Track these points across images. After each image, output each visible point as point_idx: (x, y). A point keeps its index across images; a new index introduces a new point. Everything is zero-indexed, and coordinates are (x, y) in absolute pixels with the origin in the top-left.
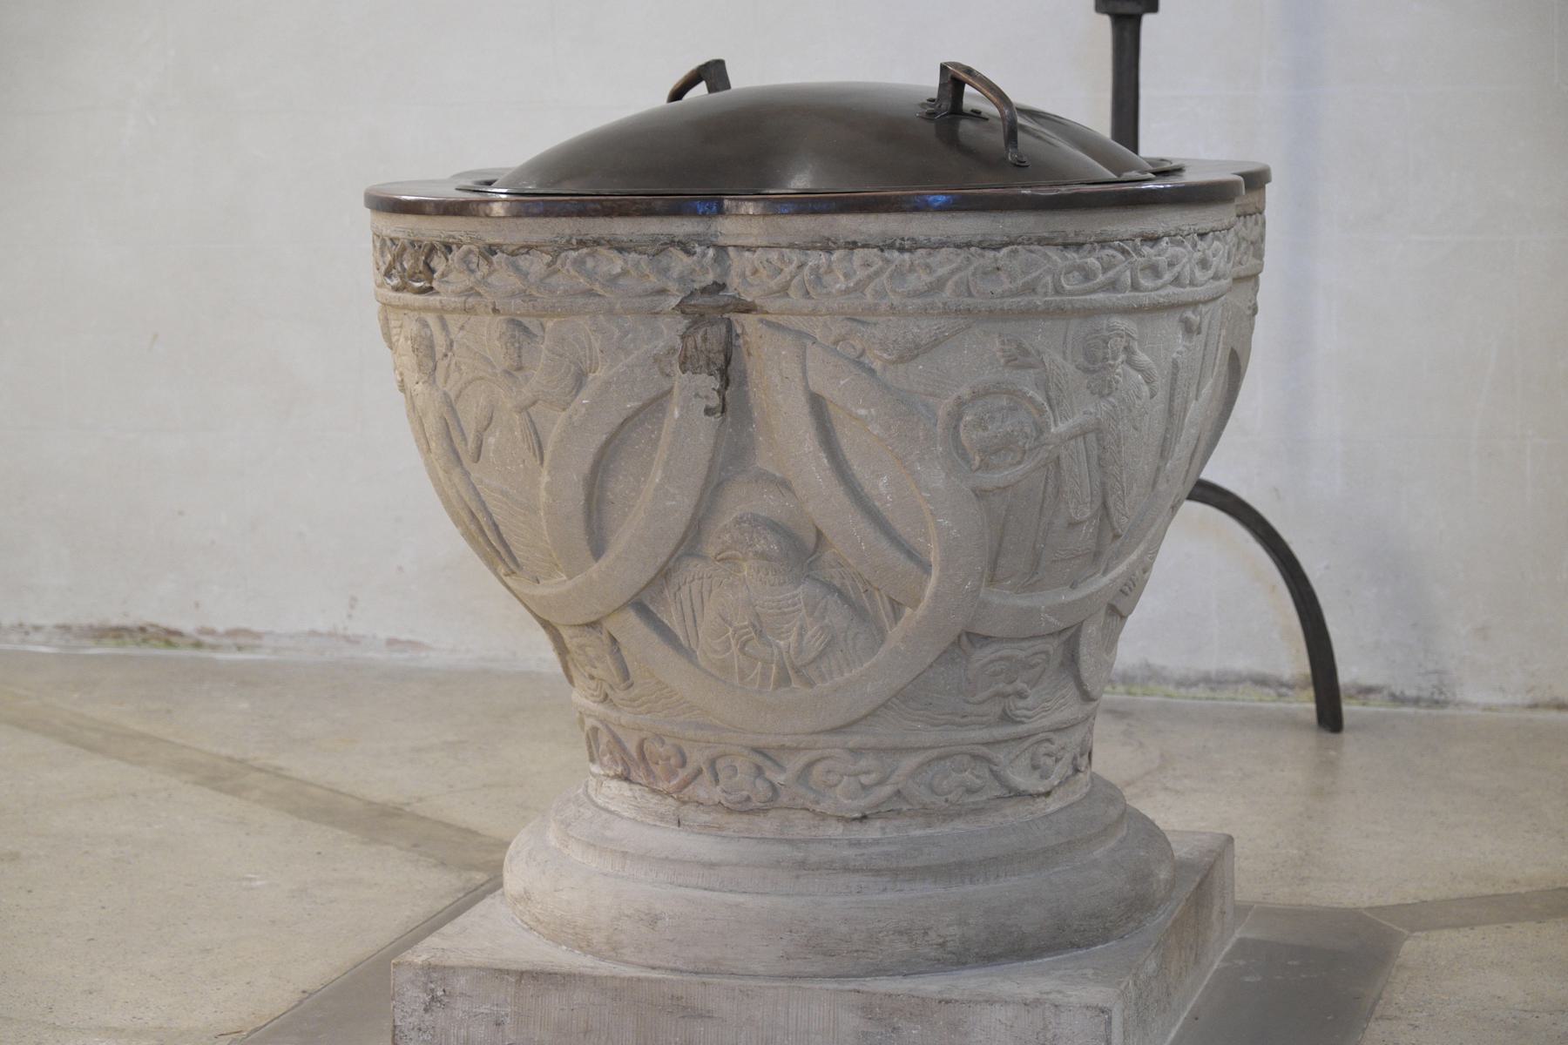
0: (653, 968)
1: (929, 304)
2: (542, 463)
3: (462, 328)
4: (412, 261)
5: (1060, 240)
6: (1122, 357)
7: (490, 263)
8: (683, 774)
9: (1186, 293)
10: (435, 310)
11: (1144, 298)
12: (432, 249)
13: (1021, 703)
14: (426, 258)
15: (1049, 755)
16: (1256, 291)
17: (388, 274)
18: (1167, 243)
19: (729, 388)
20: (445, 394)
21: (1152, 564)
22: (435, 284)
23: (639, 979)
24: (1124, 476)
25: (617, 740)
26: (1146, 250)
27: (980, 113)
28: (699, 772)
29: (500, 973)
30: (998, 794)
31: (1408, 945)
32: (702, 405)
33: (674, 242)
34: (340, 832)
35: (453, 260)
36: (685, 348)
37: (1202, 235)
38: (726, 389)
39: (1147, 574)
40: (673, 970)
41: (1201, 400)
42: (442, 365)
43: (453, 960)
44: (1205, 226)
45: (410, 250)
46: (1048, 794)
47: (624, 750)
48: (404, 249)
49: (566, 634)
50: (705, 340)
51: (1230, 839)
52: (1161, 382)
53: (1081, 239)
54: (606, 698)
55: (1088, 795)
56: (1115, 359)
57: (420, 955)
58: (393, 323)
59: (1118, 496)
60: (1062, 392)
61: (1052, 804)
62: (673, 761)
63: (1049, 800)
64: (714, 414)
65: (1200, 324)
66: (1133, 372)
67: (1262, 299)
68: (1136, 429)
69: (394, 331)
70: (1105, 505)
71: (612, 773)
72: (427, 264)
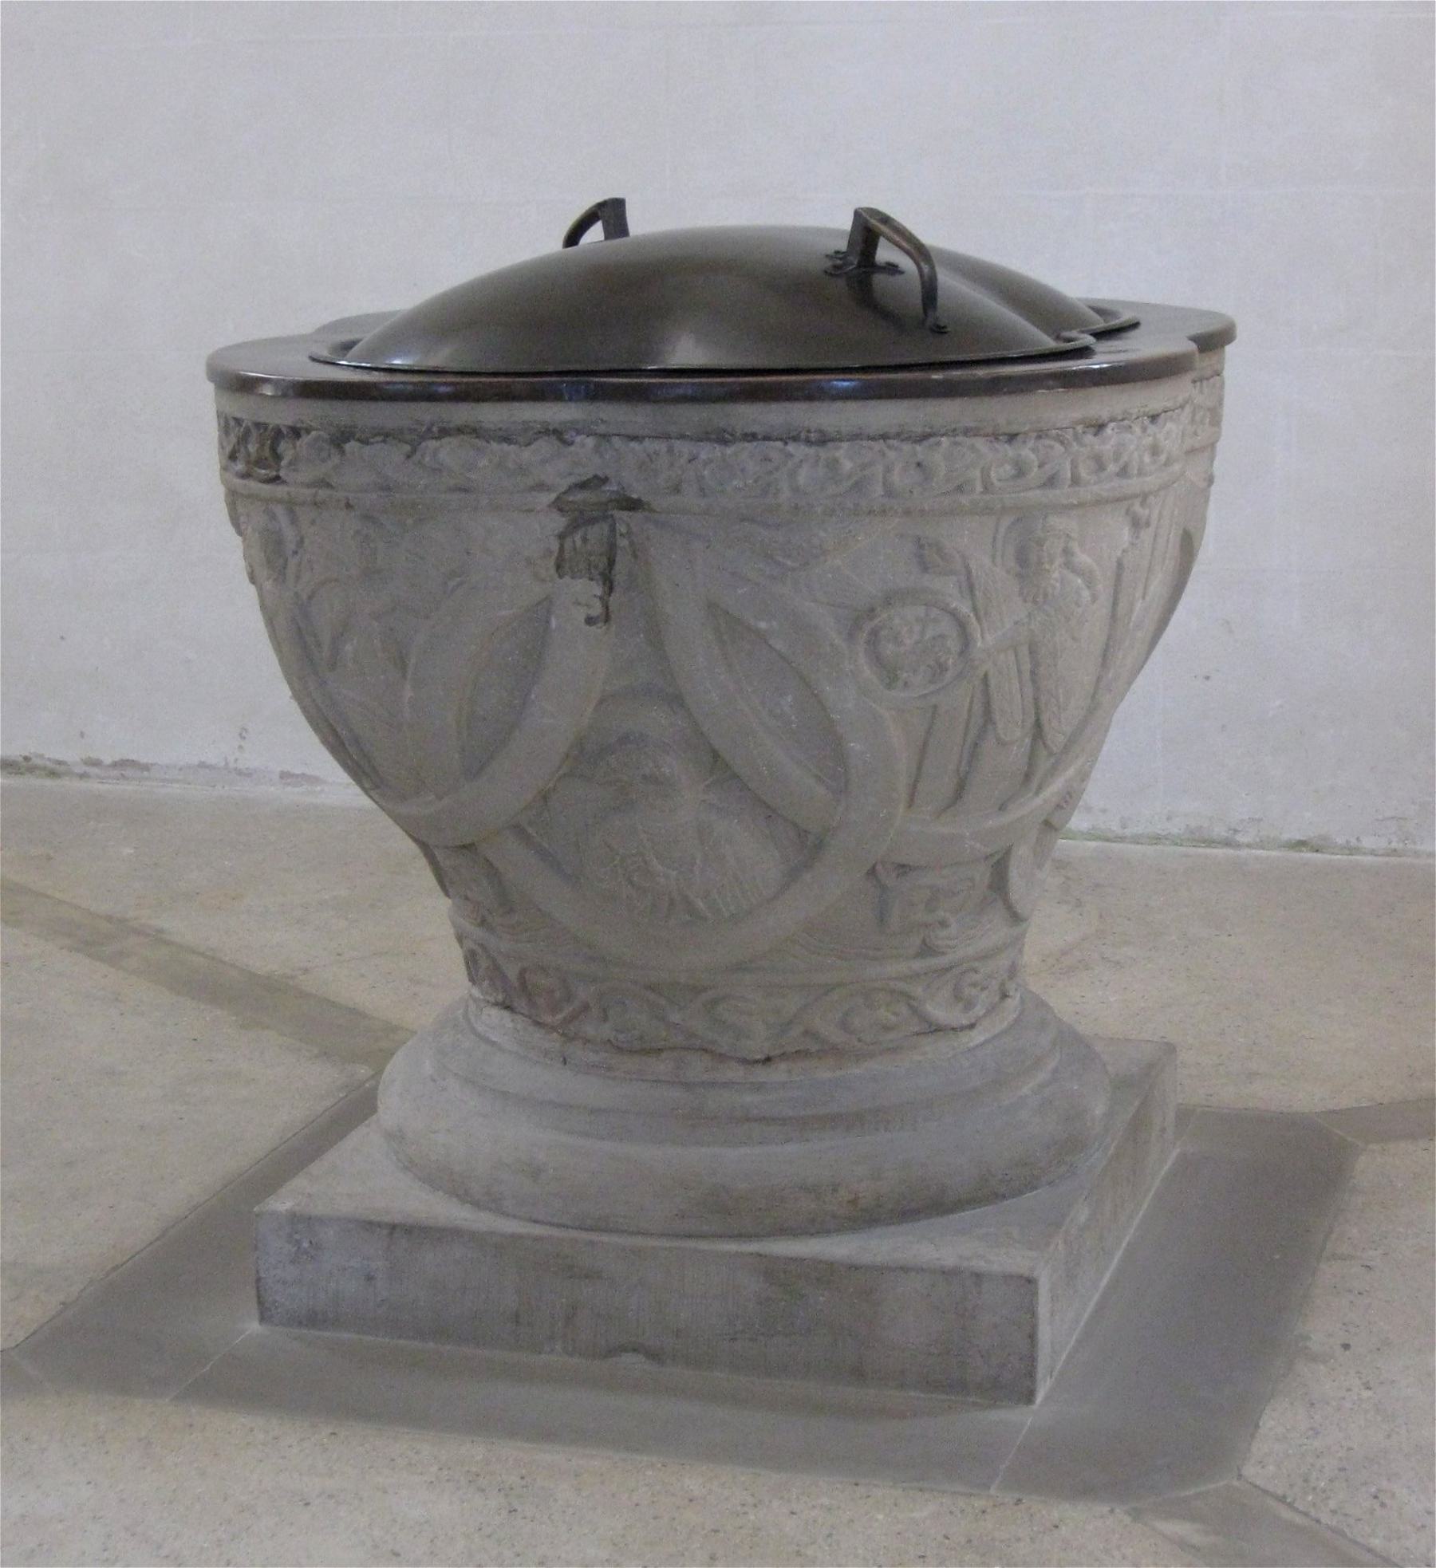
0: (536, 1222)
1: (832, 645)
2: (404, 676)
3: (313, 522)
4: (257, 445)
5: (990, 430)
6: (1059, 561)
7: (342, 452)
8: (567, 1010)
9: (1133, 484)
10: (280, 501)
11: (1085, 494)
12: (278, 434)
13: (944, 933)
14: (272, 443)
15: (974, 985)
16: (1212, 460)
17: (233, 457)
18: (1113, 429)
19: (613, 595)
20: (296, 594)
21: (1091, 772)
22: (282, 474)
23: (521, 1237)
24: (1061, 691)
25: (497, 968)
26: (1089, 438)
27: (897, 266)
28: (586, 1008)
29: (369, 1225)
30: (916, 1029)
31: (1362, 1162)
32: (580, 615)
33: (548, 430)
34: (219, 1012)
35: (300, 446)
36: (562, 549)
37: (1154, 418)
38: (610, 595)
39: (1085, 783)
40: (559, 1226)
41: (1148, 598)
42: (293, 562)
43: (320, 1209)
44: (1155, 406)
45: (254, 433)
46: (972, 1026)
47: (504, 977)
48: (247, 432)
49: (439, 855)
50: (585, 540)
51: (1170, 1049)
52: (1104, 587)
53: (1014, 429)
54: (483, 923)
55: (1017, 1021)
56: (1051, 562)
57: (282, 1203)
58: (240, 510)
59: (1053, 712)
60: (991, 601)
61: (977, 1037)
62: (558, 994)
63: (974, 1033)
64: (595, 623)
65: (1149, 516)
66: (1071, 576)
67: (1218, 467)
68: (1074, 639)
69: (242, 519)
70: (1038, 725)
71: (492, 999)
72: (273, 449)
